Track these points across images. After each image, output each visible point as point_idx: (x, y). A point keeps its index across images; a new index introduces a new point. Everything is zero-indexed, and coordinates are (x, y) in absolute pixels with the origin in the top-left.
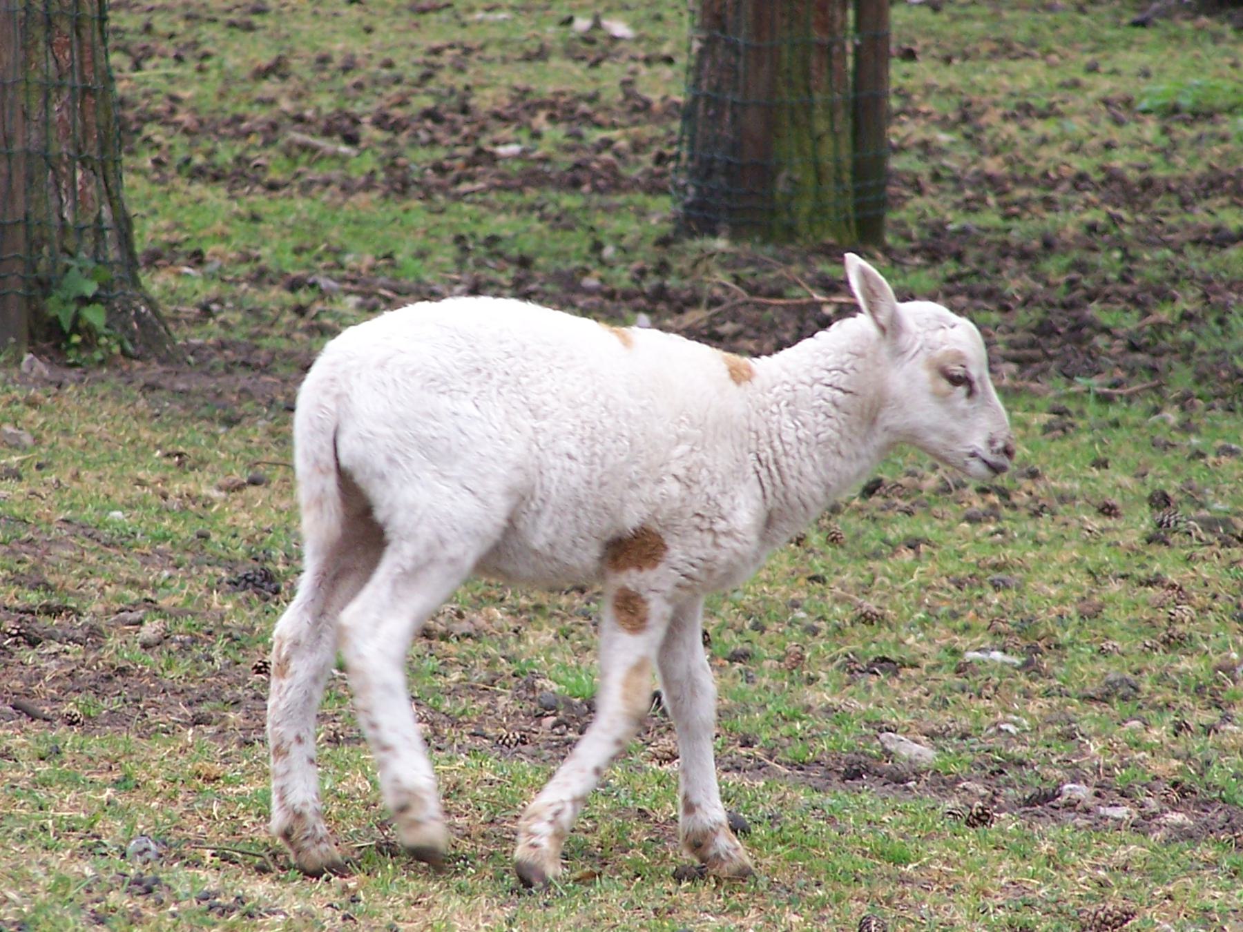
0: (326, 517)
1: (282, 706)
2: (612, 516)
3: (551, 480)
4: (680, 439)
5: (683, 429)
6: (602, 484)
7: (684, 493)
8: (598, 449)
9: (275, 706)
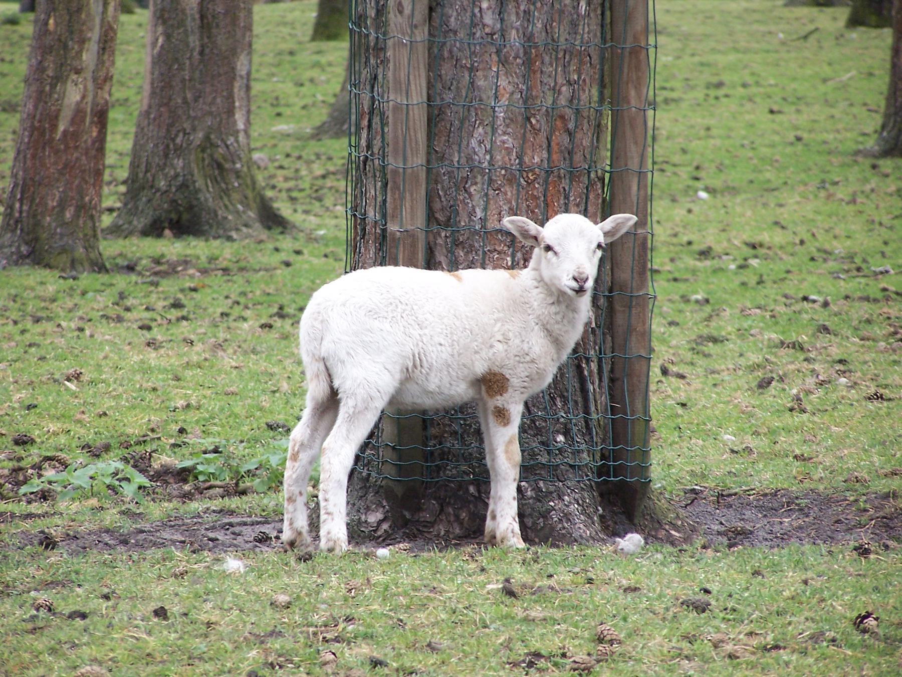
0: (322, 383)
1: (294, 476)
2: (469, 369)
3: (432, 358)
4: (497, 321)
5: (496, 316)
6: (459, 354)
7: (506, 347)
8: (455, 338)
9: (290, 476)
